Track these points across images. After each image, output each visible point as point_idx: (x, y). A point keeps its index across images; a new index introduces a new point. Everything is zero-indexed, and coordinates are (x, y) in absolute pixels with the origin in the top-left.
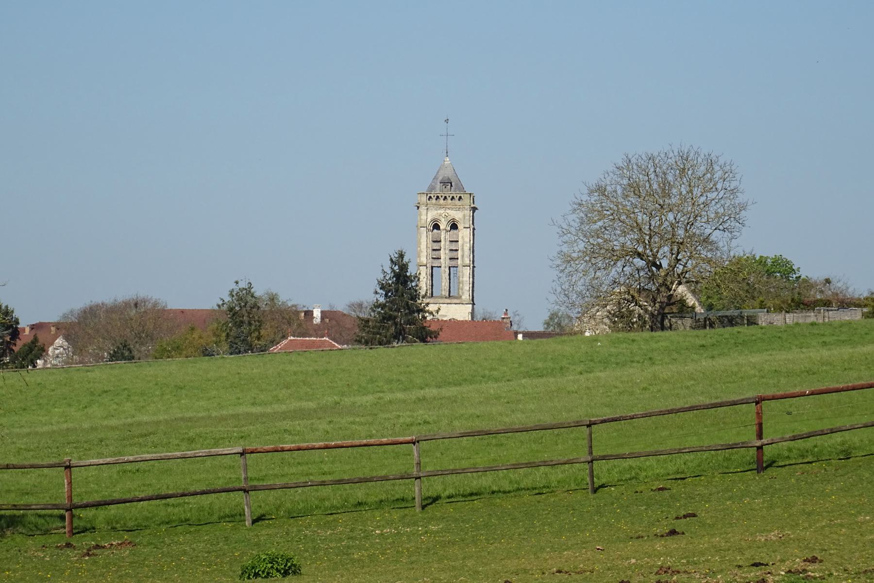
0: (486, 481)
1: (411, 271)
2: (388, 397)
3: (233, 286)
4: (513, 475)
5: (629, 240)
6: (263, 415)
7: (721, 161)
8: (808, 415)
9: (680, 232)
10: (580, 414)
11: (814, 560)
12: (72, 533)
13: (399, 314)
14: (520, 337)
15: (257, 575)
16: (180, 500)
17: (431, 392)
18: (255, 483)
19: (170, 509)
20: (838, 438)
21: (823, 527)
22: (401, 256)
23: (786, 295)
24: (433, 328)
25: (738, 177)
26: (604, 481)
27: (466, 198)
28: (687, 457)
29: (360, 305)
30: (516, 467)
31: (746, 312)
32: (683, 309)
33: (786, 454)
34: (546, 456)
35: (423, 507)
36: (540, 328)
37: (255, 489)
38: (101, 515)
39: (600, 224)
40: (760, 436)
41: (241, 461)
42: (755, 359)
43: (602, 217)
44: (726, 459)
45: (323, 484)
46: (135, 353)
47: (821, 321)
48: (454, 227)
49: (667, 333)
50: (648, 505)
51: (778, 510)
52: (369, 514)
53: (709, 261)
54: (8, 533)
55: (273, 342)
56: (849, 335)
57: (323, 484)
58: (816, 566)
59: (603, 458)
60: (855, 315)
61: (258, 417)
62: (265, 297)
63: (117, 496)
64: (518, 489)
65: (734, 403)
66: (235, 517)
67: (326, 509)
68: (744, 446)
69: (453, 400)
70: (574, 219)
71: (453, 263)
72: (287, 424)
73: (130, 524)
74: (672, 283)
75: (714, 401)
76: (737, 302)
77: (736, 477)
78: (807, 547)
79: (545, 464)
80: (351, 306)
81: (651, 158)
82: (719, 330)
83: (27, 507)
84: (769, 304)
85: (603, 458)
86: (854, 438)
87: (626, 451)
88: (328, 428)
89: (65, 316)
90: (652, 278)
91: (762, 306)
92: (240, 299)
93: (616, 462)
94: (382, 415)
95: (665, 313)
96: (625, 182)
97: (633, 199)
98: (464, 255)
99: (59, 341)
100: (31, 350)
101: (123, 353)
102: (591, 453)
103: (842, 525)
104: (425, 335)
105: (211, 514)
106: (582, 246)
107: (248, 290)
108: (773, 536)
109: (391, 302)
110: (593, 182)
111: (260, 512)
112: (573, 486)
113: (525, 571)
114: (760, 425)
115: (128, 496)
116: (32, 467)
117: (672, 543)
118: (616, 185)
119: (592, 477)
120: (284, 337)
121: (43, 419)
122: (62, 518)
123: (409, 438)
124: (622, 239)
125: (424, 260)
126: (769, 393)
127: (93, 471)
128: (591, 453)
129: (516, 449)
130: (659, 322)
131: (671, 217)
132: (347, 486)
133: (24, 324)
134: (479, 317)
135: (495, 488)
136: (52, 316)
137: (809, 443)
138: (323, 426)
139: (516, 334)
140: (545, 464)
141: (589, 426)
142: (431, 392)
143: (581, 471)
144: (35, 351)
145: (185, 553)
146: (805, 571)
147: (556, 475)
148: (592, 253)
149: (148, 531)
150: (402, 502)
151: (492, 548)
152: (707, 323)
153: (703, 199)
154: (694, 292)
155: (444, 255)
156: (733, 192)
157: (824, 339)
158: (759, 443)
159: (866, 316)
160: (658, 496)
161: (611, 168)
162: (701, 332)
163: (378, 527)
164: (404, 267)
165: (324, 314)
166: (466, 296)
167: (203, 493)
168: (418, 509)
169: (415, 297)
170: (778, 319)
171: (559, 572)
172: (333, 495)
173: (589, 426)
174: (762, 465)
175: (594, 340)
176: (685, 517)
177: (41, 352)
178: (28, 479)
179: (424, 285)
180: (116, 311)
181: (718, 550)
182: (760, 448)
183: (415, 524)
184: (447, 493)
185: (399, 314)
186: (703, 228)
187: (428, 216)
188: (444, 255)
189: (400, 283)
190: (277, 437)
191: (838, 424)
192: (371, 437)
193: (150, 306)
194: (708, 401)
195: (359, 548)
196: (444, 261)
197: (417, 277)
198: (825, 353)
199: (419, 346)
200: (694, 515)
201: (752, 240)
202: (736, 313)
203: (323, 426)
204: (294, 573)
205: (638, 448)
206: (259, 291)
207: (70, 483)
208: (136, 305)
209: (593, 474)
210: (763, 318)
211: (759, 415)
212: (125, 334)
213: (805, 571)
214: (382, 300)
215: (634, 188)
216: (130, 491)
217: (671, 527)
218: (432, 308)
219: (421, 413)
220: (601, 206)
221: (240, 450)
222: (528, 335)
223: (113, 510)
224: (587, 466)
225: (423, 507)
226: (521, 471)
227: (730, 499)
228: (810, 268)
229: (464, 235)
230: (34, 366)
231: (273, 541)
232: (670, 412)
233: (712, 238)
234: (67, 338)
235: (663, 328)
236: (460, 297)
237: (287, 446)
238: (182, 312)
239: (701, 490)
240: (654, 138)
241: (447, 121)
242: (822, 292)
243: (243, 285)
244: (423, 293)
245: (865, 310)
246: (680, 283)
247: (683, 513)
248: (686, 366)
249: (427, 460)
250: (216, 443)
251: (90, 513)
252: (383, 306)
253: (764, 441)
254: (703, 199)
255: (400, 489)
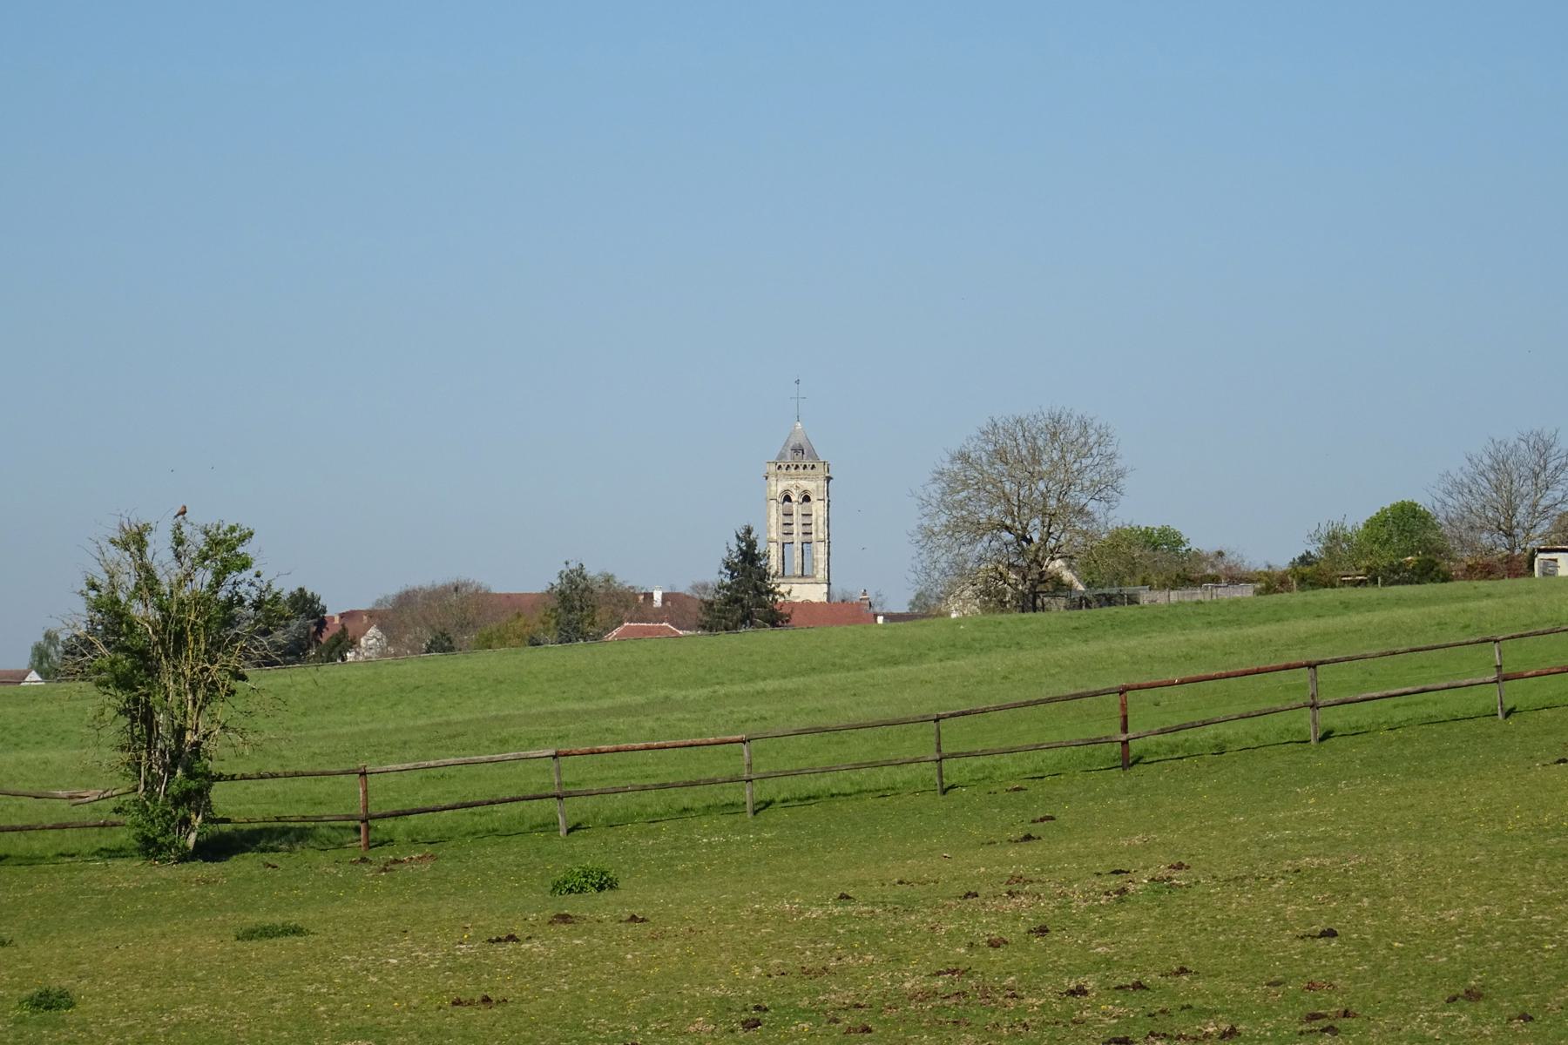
0: (825, 782)
1: (760, 549)
2: (722, 691)
3: (563, 568)
4: (854, 776)
5: (996, 513)
6: (586, 712)
7: (1096, 424)
8: (1180, 705)
9: (125, 578)
10: (930, 708)
11: (1180, 866)
12: (369, 847)
13: (746, 596)
14: (880, 620)
15: (570, 890)
16: (489, 808)
17: (771, 685)
18: (571, 789)
19: (476, 819)
20: (1210, 730)
21: (1192, 831)
22: (749, 531)
23: (1176, 569)
24: (785, 610)
25: (1115, 441)
26: (954, 781)
27: (819, 467)
28: (1045, 753)
29: (705, 587)
30: (858, 767)
31: (1127, 590)
32: (1059, 586)
33: (1154, 749)
34: (892, 755)
35: (755, 813)
36: (904, 609)
37: (570, 795)
38: (401, 825)
39: (964, 494)
40: (1125, 729)
41: (554, 763)
42: (1132, 642)
43: (966, 486)
44: (1088, 755)
45: (644, 788)
46: (456, 643)
47: (1208, 599)
48: (807, 499)
49: (1039, 615)
50: (1002, 808)
51: (1144, 812)
52: (695, 821)
53: (1085, 533)
54: (298, 848)
55: (608, 630)
56: (1237, 615)
57: (644, 788)
58: (1182, 873)
59: (953, 756)
60: (1246, 592)
61: (576, 716)
62: (601, 579)
63: (418, 805)
64: (860, 792)
65: (1096, 694)
66: (548, 826)
67: (648, 816)
68: (1109, 740)
69: (795, 693)
70: (935, 490)
71: (807, 538)
72: (606, 723)
73: (433, 836)
74: (1044, 558)
75: (1080, 691)
76: (1118, 578)
77: (1099, 775)
78: (1172, 852)
79: (889, 763)
80: (694, 588)
81: (1020, 422)
82: (1095, 611)
83: (319, 819)
84: (1154, 580)
85: (953, 756)
86: (1227, 731)
87: (979, 747)
88: (655, 725)
89: (379, 603)
90: (1022, 553)
91: (1144, 583)
92: (571, 581)
93: (968, 760)
94: (715, 712)
95: (1036, 592)
96: (990, 448)
97: (1000, 466)
98: (819, 532)
99: (372, 631)
100: (339, 642)
101: (442, 644)
102: (939, 750)
103: (1213, 828)
104: (777, 619)
105: (521, 823)
106: (944, 519)
107: (580, 572)
108: (1136, 841)
109: (738, 583)
110: (955, 448)
111: (576, 820)
112: (921, 788)
113: (864, 883)
114: (1125, 717)
115: (430, 805)
116: (323, 774)
117: (1028, 850)
118: (980, 451)
119: (941, 777)
120: (620, 623)
121: (348, 719)
122: (358, 830)
123: (738, 737)
124: (988, 511)
125: (774, 536)
126: (1137, 681)
127: (393, 778)
128: (939, 750)
129: (859, 747)
130: (1029, 602)
131: (1041, 485)
132: (672, 790)
133: (333, 611)
134: (837, 599)
135: (834, 791)
136: (364, 604)
137: (1182, 735)
138: (649, 723)
139: (876, 616)
140: (889, 763)
141: (936, 721)
142: (771, 685)
143: (930, 770)
144: (342, 644)
145: (492, 866)
146: (1169, 879)
147: (901, 775)
148: (953, 529)
149: (452, 843)
150: (732, 807)
151: (828, 857)
152: (1083, 603)
153: (1076, 466)
154: (1069, 567)
155: (797, 529)
156: (1111, 457)
157: (1211, 619)
158: (1124, 737)
159: (1258, 592)
160: (1013, 797)
161: (975, 433)
162: (1076, 612)
163: (705, 836)
164: (752, 545)
165: (665, 597)
166: (821, 575)
167: (513, 800)
168: (750, 815)
169: (764, 575)
170: (1161, 597)
171: (901, 882)
172: (655, 802)
173: (936, 721)
174: (1128, 762)
175: (957, 622)
176: (1042, 820)
177: (353, 643)
178: (323, 787)
179: (774, 564)
180: (436, 596)
181: (1077, 856)
182: (1125, 743)
183: (746, 831)
184: (782, 796)
185: (746, 596)
186: (1077, 497)
187: (778, 487)
188: (797, 529)
189: (748, 562)
190: (598, 736)
191: (1212, 715)
192: (701, 735)
193: (472, 590)
194: (1072, 692)
195: (683, 859)
196: (797, 538)
197: (766, 555)
198: (1085, 648)
199: (769, 635)
200: (1052, 818)
201: (1133, 509)
202: (1115, 591)
203: (649, 723)
204: (611, 887)
205: (994, 744)
206: (592, 571)
207: (365, 792)
208: (456, 589)
209: (942, 774)
210: (1145, 597)
211: (1124, 706)
212: (444, 623)
213: (1169, 879)
214: (727, 581)
215: (1000, 455)
216: (432, 799)
217: (1026, 832)
218: (783, 589)
219: (759, 709)
220: (963, 476)
221: (553, 752)
222: (890, 617)
223: (414, 819)
224: (935, 765)
225: (755, 813)
226: (864, 772)
227: (1092, 799)
228: (1200, 539)
229: (818, 508)
230: (344, 659)
231: (591, 852)
232: (1027, 704)
233: (1087, 509)
234: (381, 627)
235: (1035, 609)
236: (813, 576)
237: (604, 747)
238: (508, 596)
239: (1061, 789)
240: (1026, 398)
241: (798, 382)
242: (1213, 566)
243: (574, 566)
244: (773, 572)
245: (1258, 586)
246: (1052, 559)
247: (1040, 815)
248: (1067, 651)
249: (761, 760)
250: (532, 744)
251: (388, 824)
252: (729, 588)
253: (1130, 735)
254: (1076, 466)
255: (730, 794)
